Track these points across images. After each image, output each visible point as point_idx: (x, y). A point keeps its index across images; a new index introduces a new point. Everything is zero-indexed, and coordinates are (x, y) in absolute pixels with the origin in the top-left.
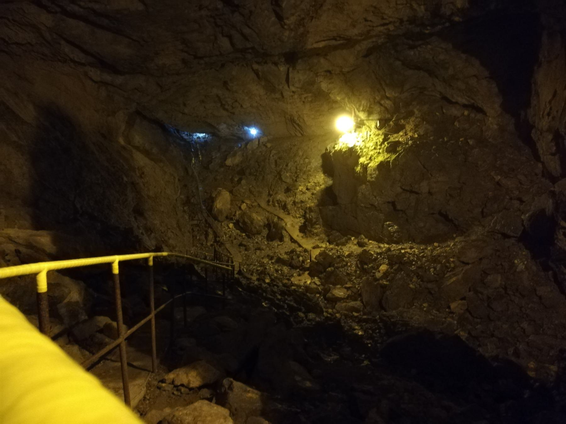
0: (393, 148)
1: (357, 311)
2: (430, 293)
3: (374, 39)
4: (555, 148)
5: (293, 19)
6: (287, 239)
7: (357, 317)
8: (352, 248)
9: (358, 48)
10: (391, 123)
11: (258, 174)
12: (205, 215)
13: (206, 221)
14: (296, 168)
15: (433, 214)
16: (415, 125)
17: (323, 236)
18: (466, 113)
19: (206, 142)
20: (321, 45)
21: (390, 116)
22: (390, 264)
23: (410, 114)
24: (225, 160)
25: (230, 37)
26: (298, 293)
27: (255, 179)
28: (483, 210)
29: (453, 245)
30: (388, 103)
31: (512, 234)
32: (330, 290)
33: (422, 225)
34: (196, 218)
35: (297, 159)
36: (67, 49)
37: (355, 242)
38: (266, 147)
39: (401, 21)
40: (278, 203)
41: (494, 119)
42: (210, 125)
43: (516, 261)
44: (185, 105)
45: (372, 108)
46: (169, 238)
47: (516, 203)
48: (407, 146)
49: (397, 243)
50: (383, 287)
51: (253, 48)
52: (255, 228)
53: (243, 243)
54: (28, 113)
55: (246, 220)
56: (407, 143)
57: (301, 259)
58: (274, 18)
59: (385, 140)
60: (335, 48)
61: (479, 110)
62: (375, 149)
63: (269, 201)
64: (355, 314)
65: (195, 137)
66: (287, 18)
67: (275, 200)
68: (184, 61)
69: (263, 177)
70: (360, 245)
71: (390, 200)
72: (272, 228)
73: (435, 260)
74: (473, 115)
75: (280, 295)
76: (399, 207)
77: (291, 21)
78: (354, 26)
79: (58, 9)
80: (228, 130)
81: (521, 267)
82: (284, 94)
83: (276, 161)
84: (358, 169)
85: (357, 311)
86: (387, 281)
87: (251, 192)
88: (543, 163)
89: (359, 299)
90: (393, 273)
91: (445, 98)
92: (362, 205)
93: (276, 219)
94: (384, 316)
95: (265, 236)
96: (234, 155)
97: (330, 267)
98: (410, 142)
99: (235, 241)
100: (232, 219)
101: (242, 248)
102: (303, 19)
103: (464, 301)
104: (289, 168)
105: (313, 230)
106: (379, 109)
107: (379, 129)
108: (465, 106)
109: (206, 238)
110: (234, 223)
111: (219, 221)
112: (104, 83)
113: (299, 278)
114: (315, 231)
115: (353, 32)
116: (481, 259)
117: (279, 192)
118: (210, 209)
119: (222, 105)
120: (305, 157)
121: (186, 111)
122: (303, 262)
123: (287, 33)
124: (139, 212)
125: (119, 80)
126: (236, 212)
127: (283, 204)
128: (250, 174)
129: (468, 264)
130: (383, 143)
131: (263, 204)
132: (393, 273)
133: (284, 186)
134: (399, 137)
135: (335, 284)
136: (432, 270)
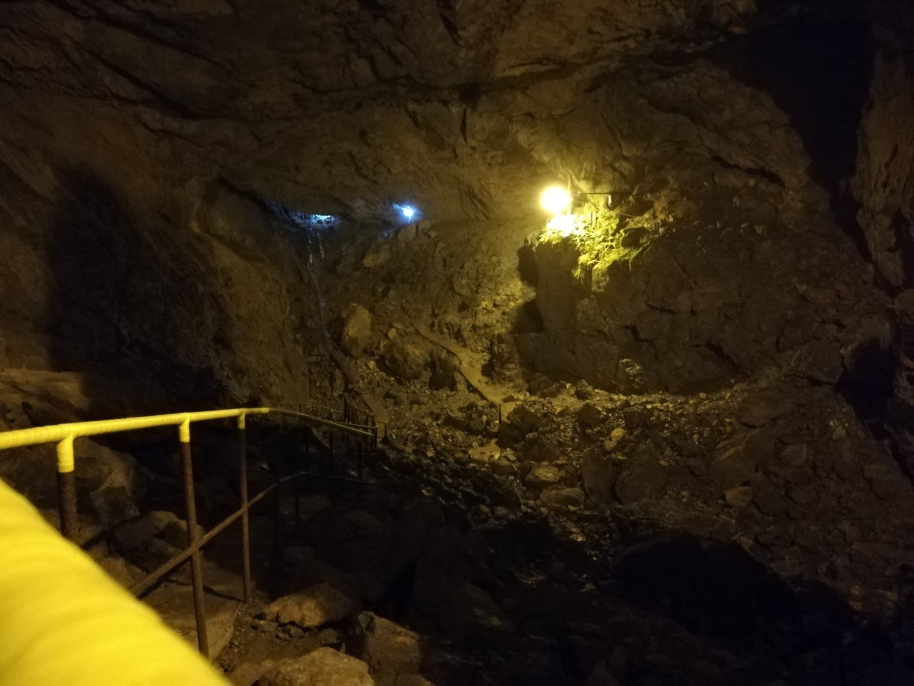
0: (633, 239)
1: (575, 502)
2: (692, 473)
3: (603, 63)
4: (894, 240)
5: (473, 29)
6: (461, 387)
7: (574, 513)
8: (566, 400)
9: (577, 76)
10: (631, 198)
11: (415, 281)
12: (330, 347)
13: (331, 357)
14: (478, 271)
17: (520, 381)
18: (752, 182)
19: (331, 229)
20: (517, 72)
21: (628, 187)
22: (629, 428)
23: (662, 184)
24: (363, 258)
25: (371, 60)
26: (479, 475)
27: (410, 290)
28: (778, 339)
29: (731, 396)
30: (625, 167)
31: (825, 379)
33: (679, 363)
34: (316, 352)
35: (479, 256)
36: (107, 77)
37: (572, 391)
38: (429, 237)
39: (648, 33)
40: (448, 328)
41: (796, 192)
42: (338, 202)
43: (831, 423)
44: (297, 168)
45: (599, 174)
46: (271, 385)
47: (832, 329)
48: (657, 236)
49: (640, 393)
50: (617, 464)
51: (407, 77)
52: (411, 368)
53: (391, 392)
54: (44, 181)
55: (396, 355)
56: (656, 232)
57: (484, 418)
58: (441, 29)
59: (620, 226)
60: (541, 77)
61: (774, 178)
62: (604, 240)
63: (432, 325)
64: (572, 508)
66: (464, 29)
67: (443, 323)
68: (296, 98)
69: (424, 286)
70: (581, 396)
71: (628, 323)
72: (438, 368)
73: (701, 420)
74: (762, 186)
75: (451, 477)
76: (642, 336)
77: (470, 32)
78: (572, 42)
79: (92, 13)
80: (366, 210)
81: (840, 432)
82: (459, 152)
83: (444, 260)
84: (578, 273)
85: (575, 502)
86: (623, 455)
87: (403, 309)
88: (875, 264)
89: (578, 483)
90: (633, 442)
91: (718, 159)
92: (584, 331)
93: (444, 354)
94: (619, 511)
95: (427, 381)
96: (377, 250)
97: (531, 431)
98: (661, 230)
99: (378, 390)
100: (373, 354)
101: (390, 401)
102: (489, 29)
103: (746, 488)
104: (465, 272)
105: (504, 371)
106: (611, 176)
107: (611, 208)
108: (750, 172)
109: (331, 384)
110: (376, 361)
111: (352, 357)
112: (167, 133)
113: (482, 449)
114: (508, 373)
115: (571, 51)
117: (450, 310)
118: (338, 338)
119: (358, 169)
120: (491, 253)
121: (299, 178)
122: (488, 423)
123: (463, 53)
124: (222, 342)
125: (192, 127)
126: (379, 343)
127: (456, 329)
128: (404, 281)
129: (754, 427)
130: (617, 231)
131: (424, 330)
132: (633, 442)
133: (458, 301)
134: (643, 221)
135: (539, 460)
136: (696, 436)
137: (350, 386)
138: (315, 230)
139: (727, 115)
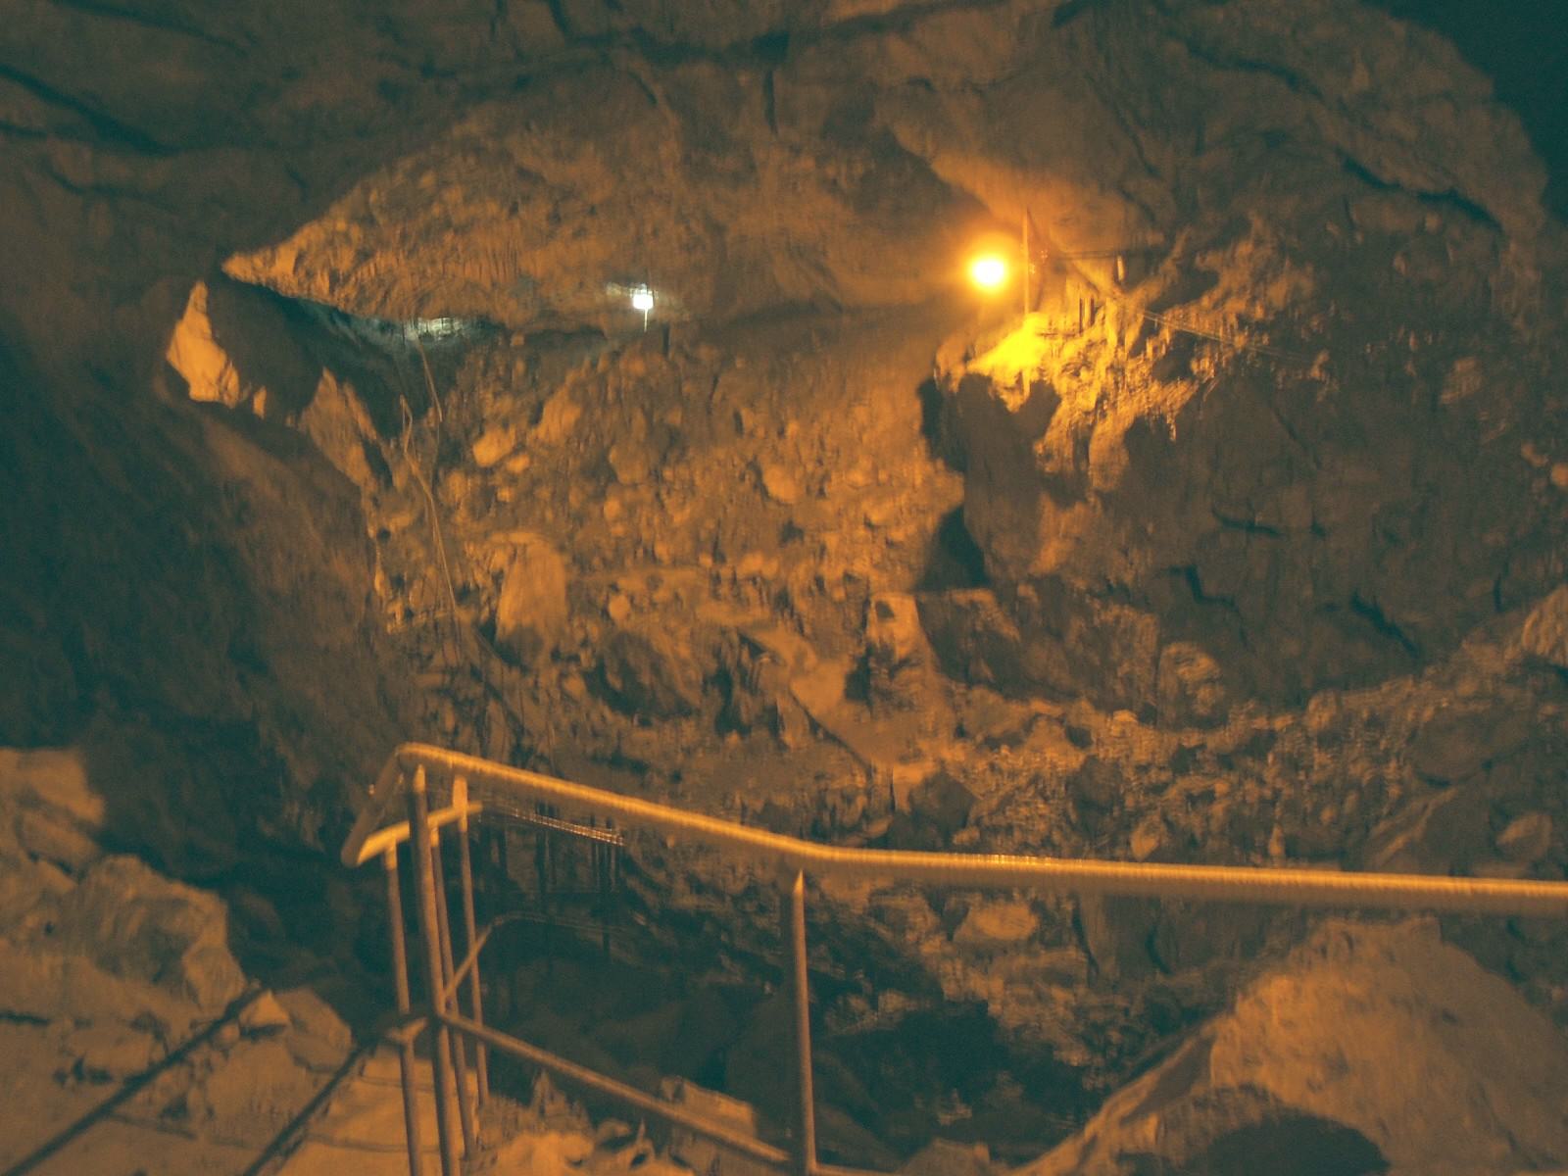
15: (1331, 607)
16: (1252, 275)
18: (1432, 222)
23: (1233, 231)
32: (966, 911)
59: (1149, 330)
61: (1478, 214)
65: (412, 334)
70: (1078, 738)
76: (1210, 587)
91: (1352, 167)
108: (1428, 199)
110: (586, 676)
116: (1488, 765)
129: (1443, 784)
134: (1198, 320)
137: (461, 697)
138: (415, 358)
139: (1361, 80)
